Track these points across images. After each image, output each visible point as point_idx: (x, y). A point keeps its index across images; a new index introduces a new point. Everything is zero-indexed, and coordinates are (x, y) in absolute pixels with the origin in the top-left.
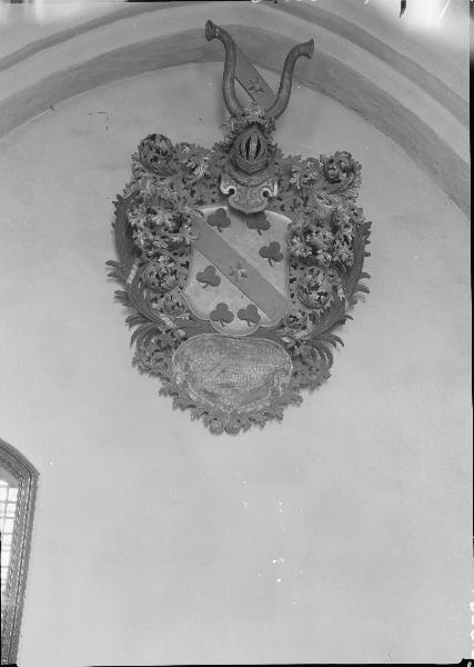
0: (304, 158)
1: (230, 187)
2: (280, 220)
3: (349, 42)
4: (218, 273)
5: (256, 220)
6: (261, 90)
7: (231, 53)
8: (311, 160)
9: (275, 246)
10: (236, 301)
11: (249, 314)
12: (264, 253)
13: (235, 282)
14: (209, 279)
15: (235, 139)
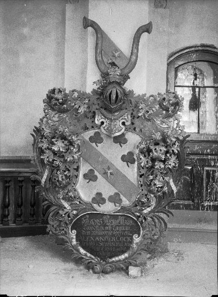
0: (148, 95)
1: (101, 121)
2: (133, 139)
3: (14, 238)
4: (96, 173)
5: (120, 140)
6: (119, 57)
7: (136, 51)
8: (152, 96)
9: (131, 154)
10: (108, 191)
11: (115, 199)
12: (123, 158)
13: (107, 179)
14: (90, 177)
15: (103, 90)
